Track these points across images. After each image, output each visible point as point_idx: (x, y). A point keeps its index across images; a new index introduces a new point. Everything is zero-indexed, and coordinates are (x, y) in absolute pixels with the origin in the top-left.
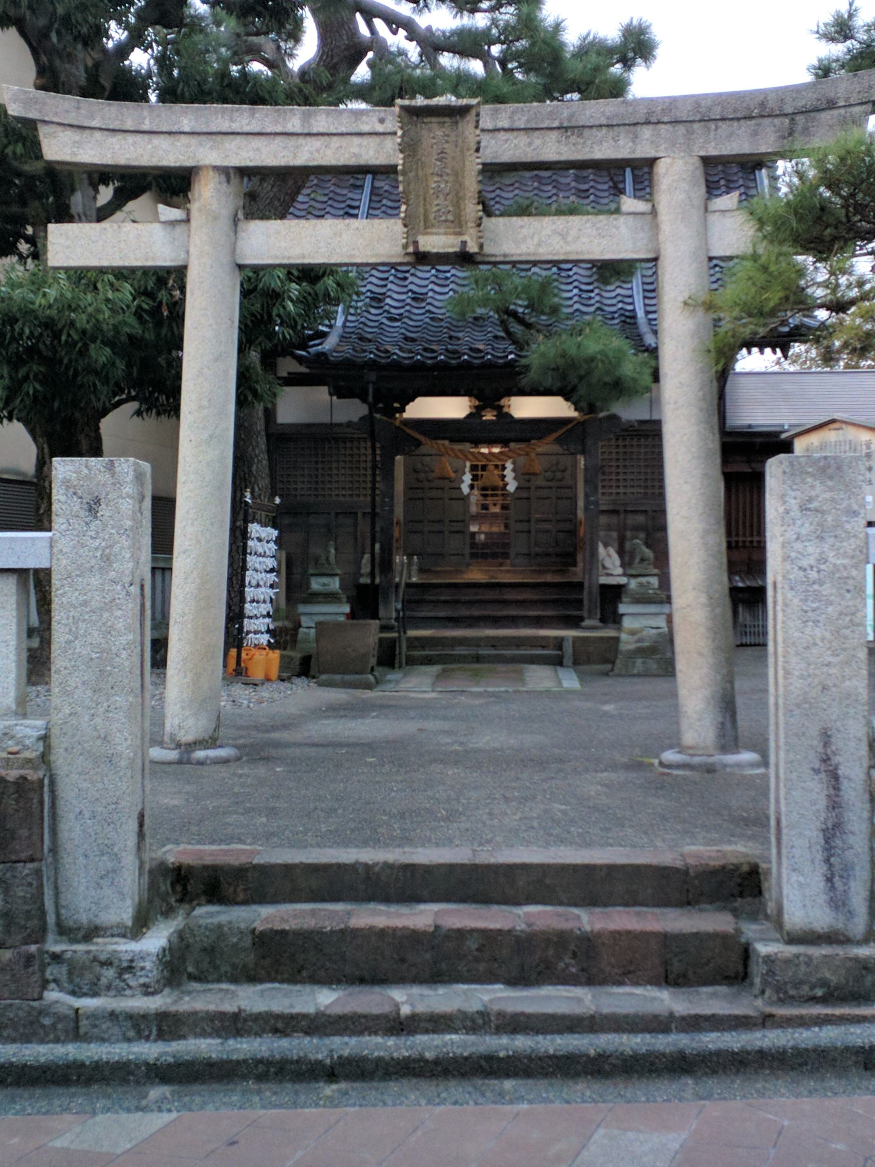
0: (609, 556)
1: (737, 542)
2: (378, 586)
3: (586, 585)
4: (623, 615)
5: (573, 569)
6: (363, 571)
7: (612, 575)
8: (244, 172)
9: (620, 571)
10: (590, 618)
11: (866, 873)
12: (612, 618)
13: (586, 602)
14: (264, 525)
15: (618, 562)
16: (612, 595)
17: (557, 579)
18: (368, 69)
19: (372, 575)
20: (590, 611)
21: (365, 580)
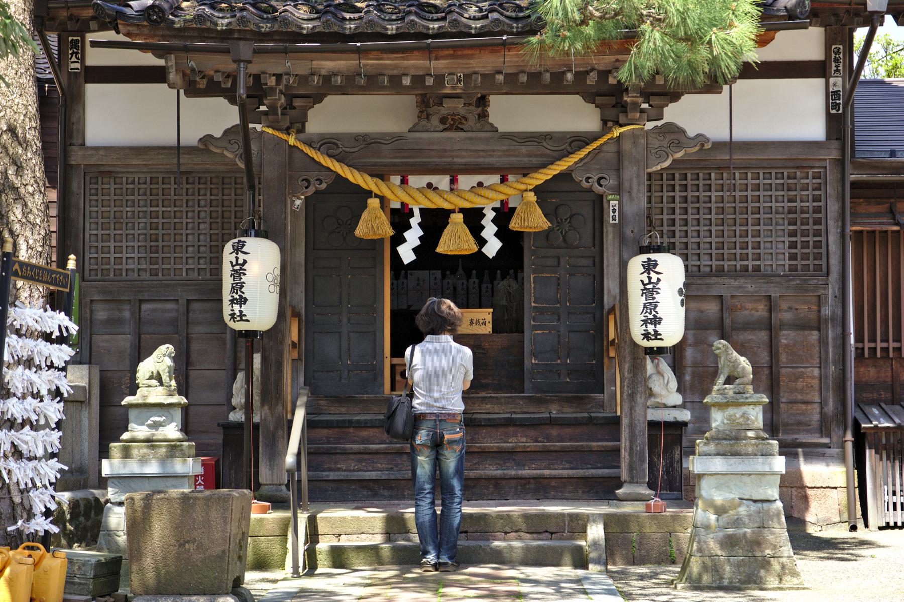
0: (660, 373)
1: (885, 350)
2: (256, 427)
3: (625, 422)
4: (700, 477)
5: (598, 396)
6: (234, 401)
7: (666, 406)
8: (762, 589)
9: (677, 399)
10: (632, 481)
11: (704, 493)
12: (678, 487)
13: (624, 454)
14: (690, 294)
15: (674, 384)
16: (670, 439)
17: (569, 412)
18: (589, 531)
19: (248, 407)
20: (631, 469)
21: (236, 416)
